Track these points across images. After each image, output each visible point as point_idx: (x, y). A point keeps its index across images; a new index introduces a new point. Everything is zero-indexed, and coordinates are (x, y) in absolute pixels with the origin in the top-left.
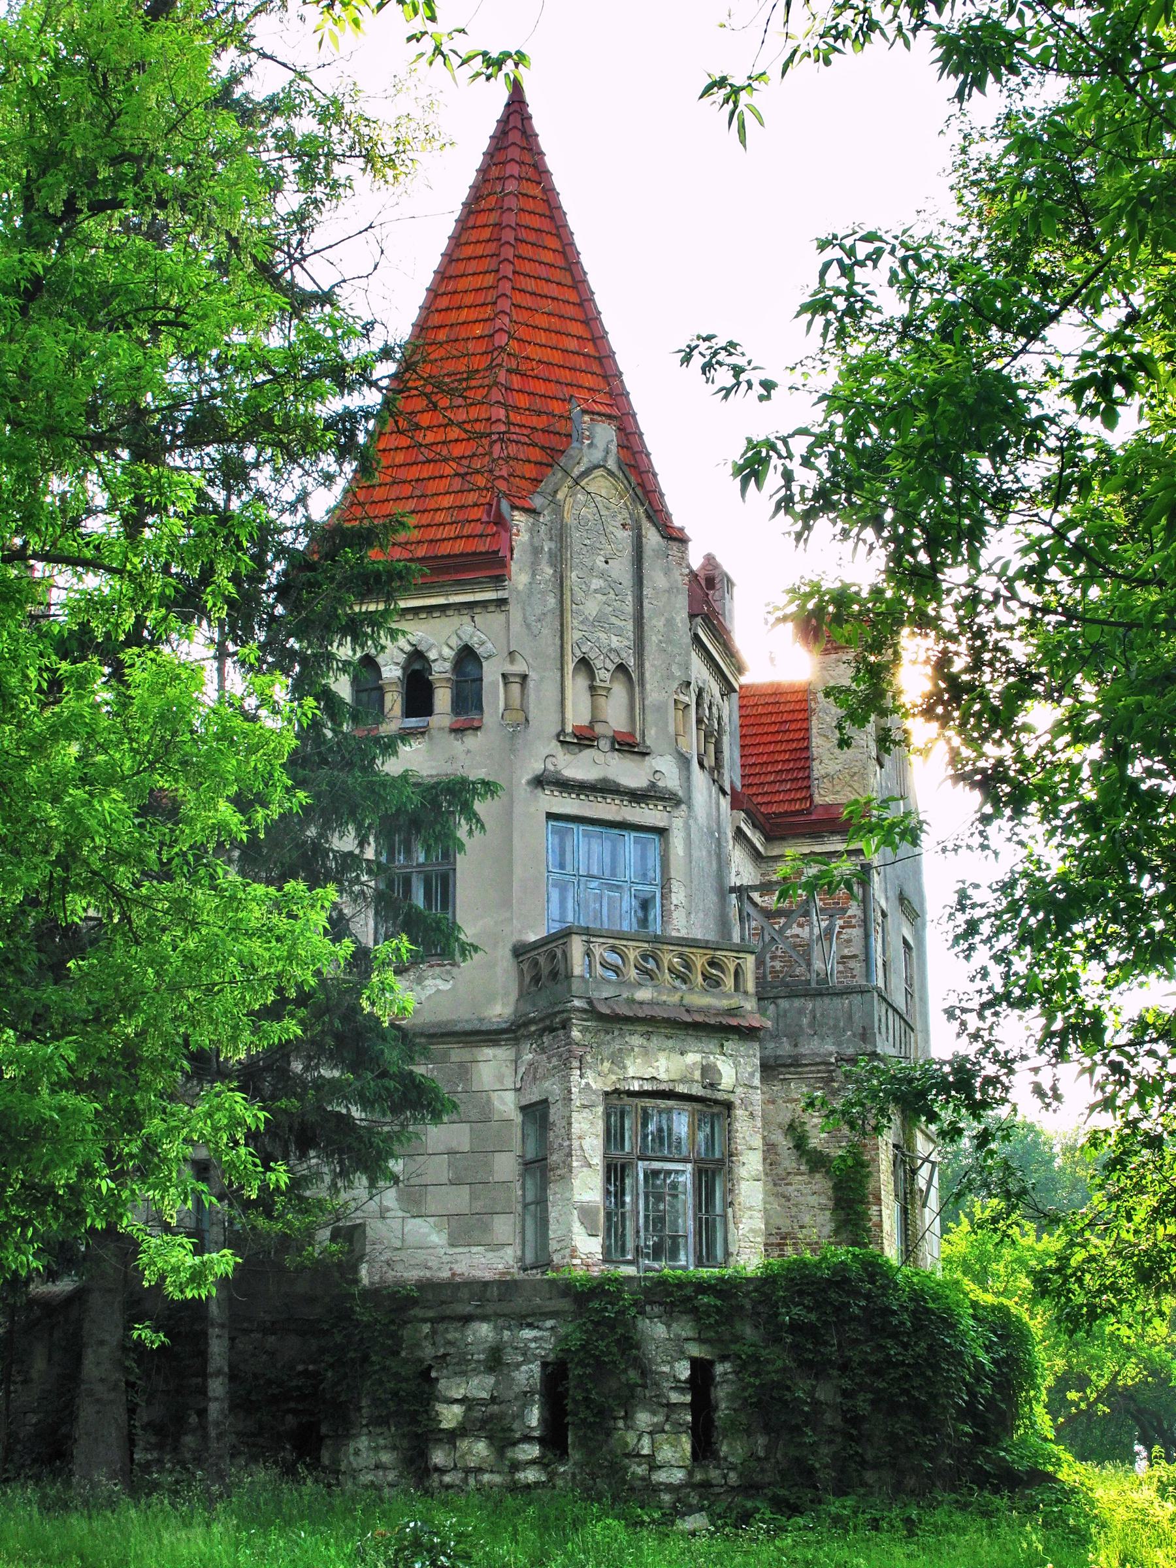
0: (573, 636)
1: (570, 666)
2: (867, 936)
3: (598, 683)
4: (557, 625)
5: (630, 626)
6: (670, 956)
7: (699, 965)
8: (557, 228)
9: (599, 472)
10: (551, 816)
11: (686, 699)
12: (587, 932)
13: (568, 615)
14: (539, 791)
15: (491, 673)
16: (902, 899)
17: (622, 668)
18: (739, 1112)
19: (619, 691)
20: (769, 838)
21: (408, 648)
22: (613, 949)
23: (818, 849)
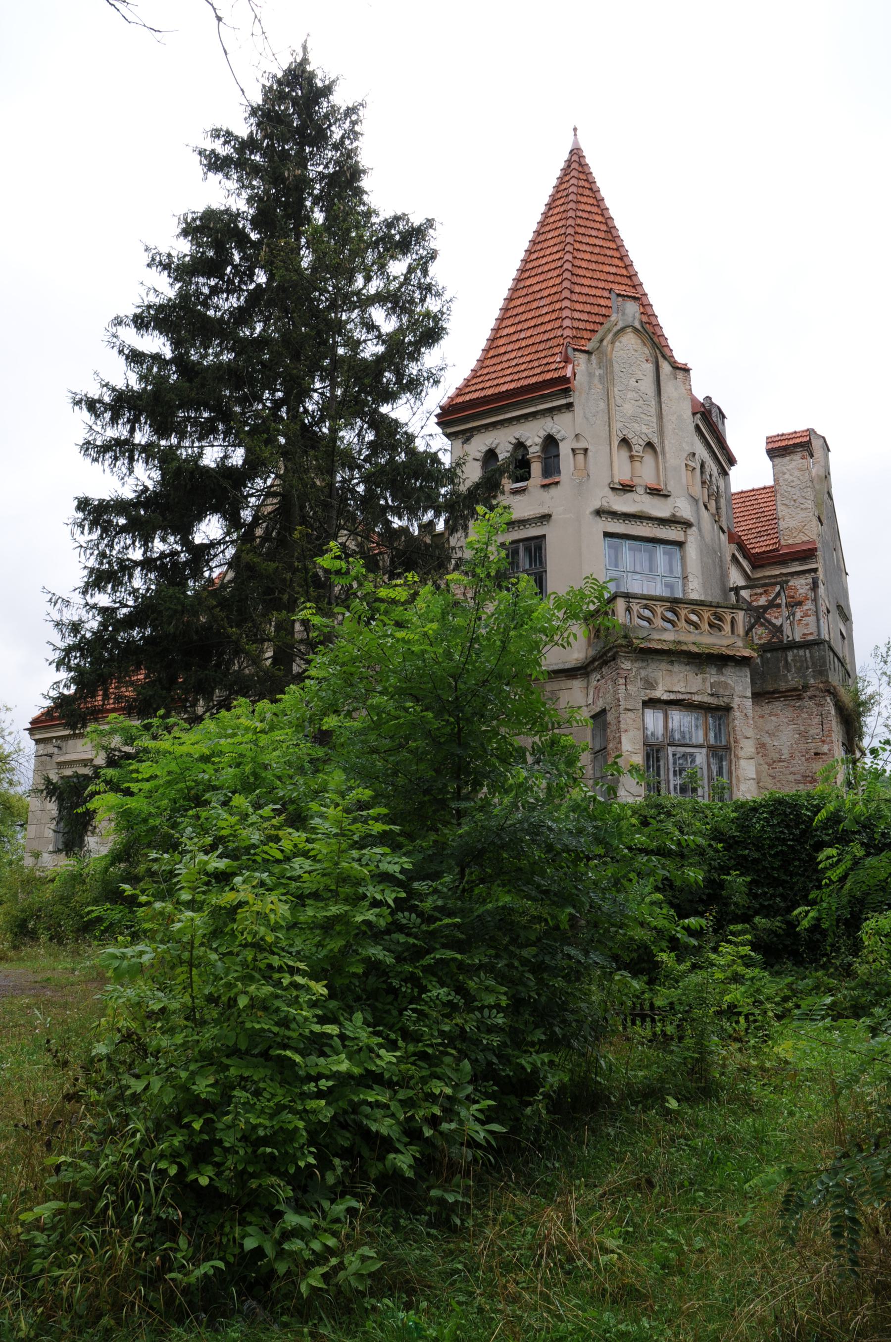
0: (617, 425)
1: (616, 443)
2: (818, 620)
3: (634, 453)
4: (606, 418)
5: (654, 420)
6: (686, 611)
7: (706, 617)
8: (598, 201)
9: (629, 330)
10: (607, 535)
11: (693, 464)
12: (628, 596)
13: (613, 412)
14: (598, 518)
15: (565, 449)
16: (839, 607)
17: (650, 445)
18: (737, 714)
19: (649, 458)
20: (754, 567)
21: (514, 441)
22: (646, 607)
23: (785, 571)
